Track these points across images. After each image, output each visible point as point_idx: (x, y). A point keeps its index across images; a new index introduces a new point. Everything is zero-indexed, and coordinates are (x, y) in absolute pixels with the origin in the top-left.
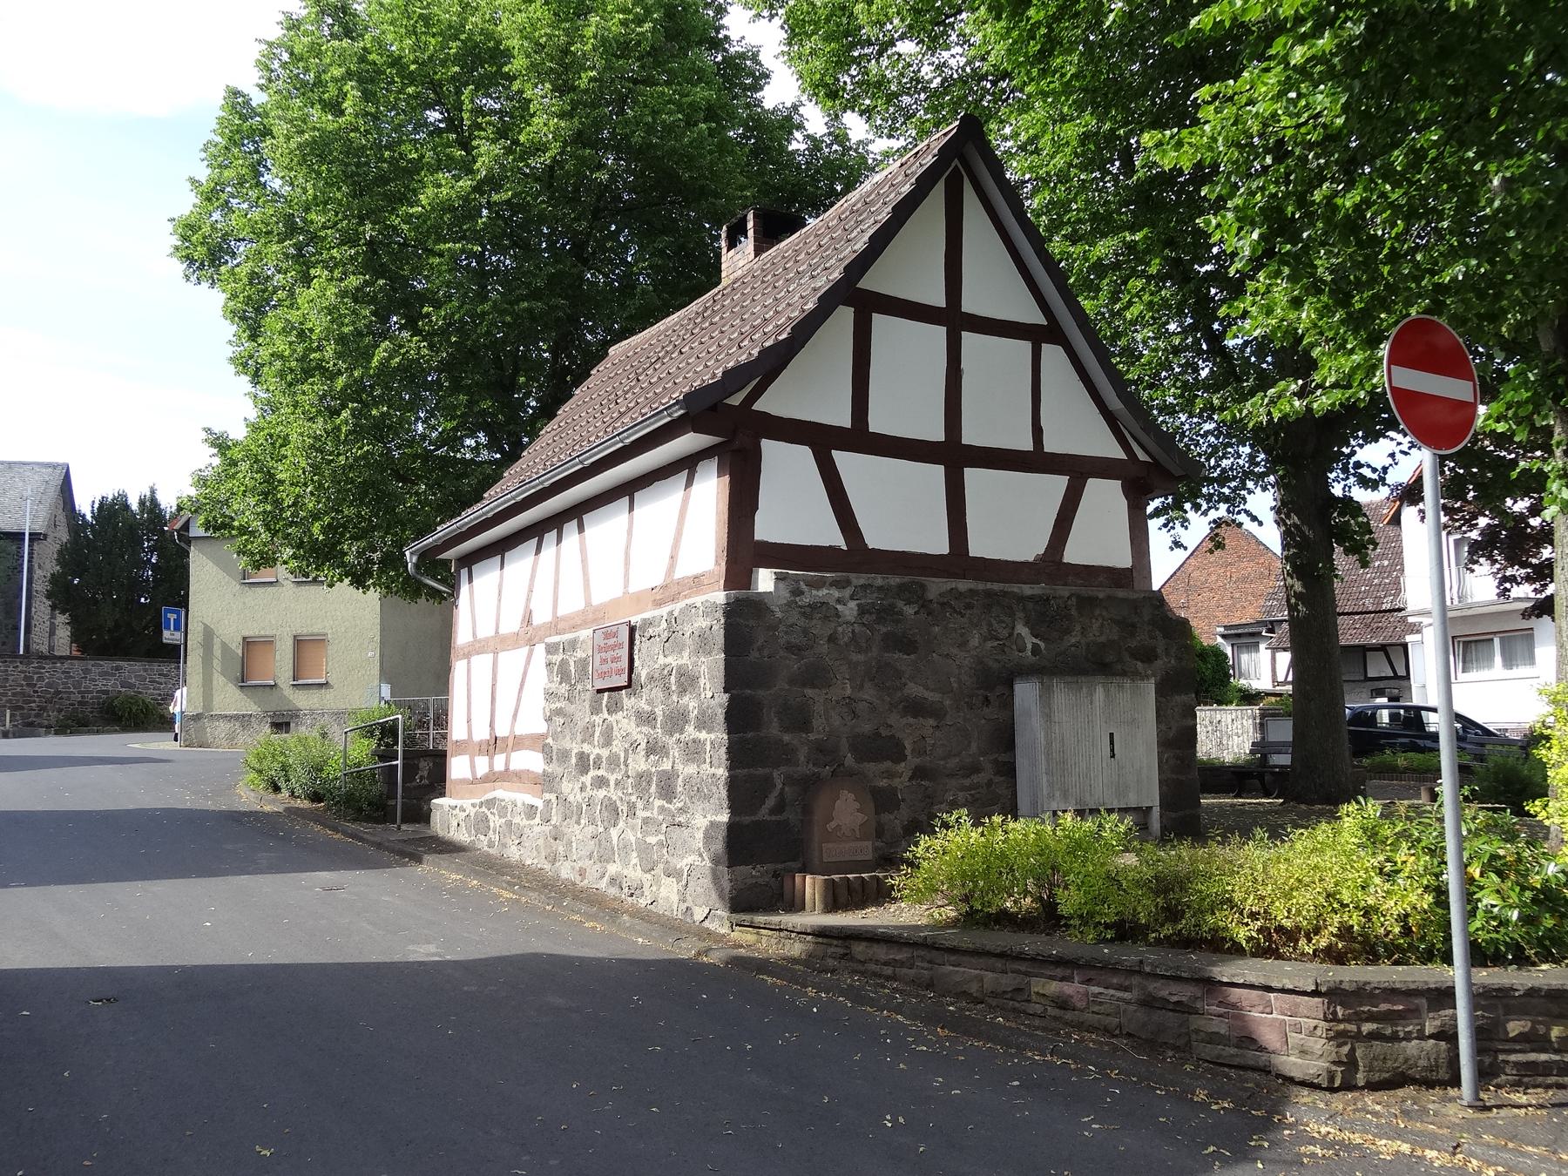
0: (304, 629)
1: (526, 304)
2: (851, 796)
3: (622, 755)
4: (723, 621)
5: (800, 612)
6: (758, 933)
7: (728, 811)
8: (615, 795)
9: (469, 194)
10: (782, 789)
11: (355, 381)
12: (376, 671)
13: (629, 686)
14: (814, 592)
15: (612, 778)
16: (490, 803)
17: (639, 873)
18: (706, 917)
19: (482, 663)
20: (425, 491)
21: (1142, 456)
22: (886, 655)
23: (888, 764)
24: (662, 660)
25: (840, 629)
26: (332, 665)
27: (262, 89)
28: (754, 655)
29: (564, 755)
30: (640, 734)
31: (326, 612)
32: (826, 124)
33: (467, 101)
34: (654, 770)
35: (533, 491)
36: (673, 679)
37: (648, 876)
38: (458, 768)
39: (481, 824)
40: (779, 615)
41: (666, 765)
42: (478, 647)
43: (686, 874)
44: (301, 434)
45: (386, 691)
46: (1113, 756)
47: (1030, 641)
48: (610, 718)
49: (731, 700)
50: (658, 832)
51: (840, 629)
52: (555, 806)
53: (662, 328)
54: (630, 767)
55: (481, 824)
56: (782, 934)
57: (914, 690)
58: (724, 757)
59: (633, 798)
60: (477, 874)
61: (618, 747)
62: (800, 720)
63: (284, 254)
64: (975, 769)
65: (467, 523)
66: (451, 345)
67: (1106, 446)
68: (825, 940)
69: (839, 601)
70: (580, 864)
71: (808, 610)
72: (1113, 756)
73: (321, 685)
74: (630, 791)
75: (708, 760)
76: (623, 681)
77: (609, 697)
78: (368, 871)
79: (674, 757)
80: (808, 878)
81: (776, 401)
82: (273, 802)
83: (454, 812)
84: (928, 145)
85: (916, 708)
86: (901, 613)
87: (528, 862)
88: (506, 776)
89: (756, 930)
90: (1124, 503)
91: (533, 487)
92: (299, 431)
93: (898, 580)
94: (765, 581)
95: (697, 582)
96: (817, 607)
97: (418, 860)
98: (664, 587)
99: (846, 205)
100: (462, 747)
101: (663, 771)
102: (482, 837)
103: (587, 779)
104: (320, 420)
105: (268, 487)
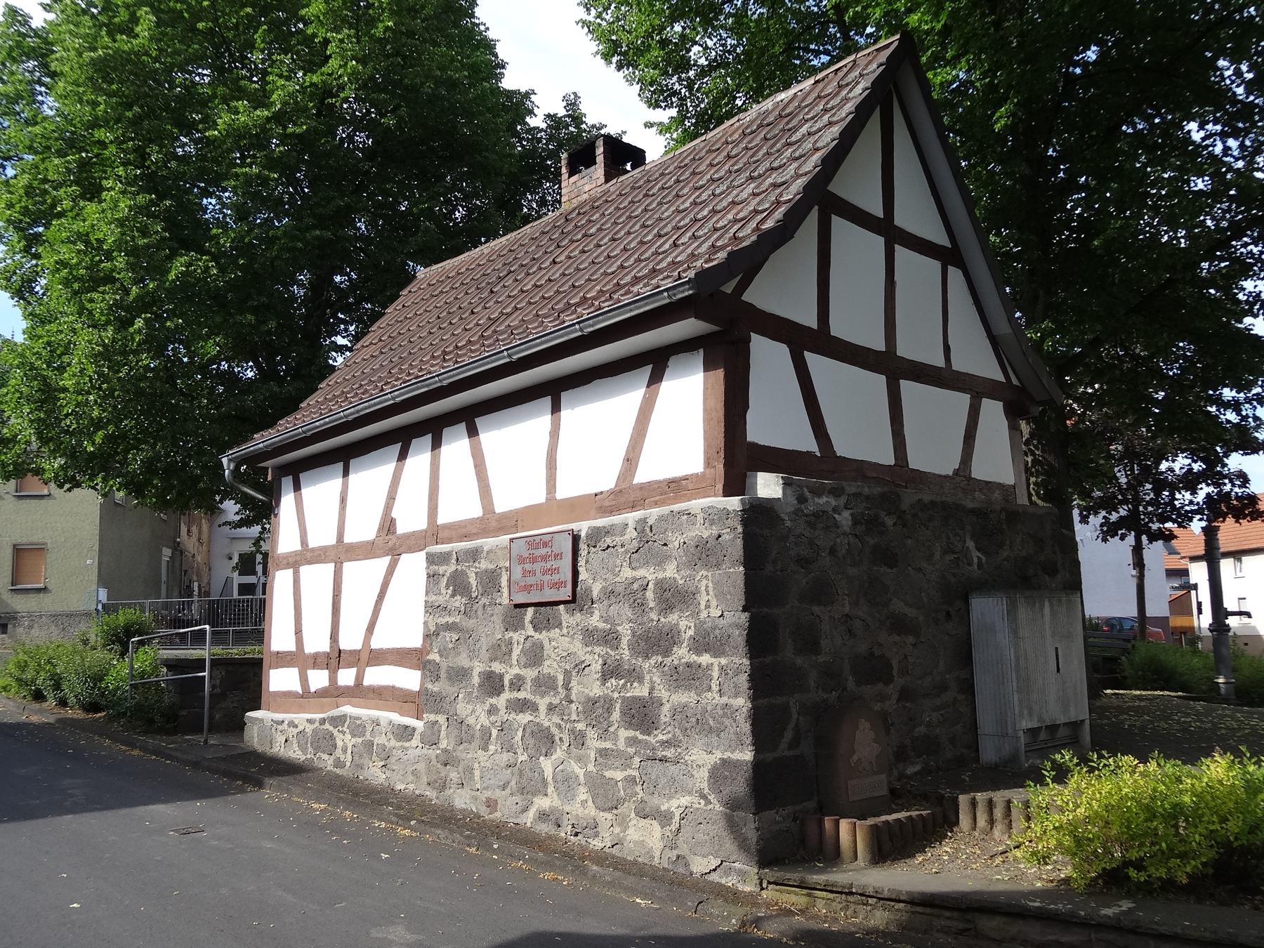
0: (23, 538)
1: (318, 232)
2: (867, 725)
3: (560, 678)
4: (740, 529)
5: (806, 522)
6: (809, 895)
7: (751, 748)
8: (544, 719)
9: (265, 124)
10: (798, 719)
11: (148, 293)
12: (94, 577)
13: (573, 600)
14: (816, 500)
16: (338, 721)
17: (591, 810)
18: (714, 870)
19: (317, 577)
20: (207, 405)
21: (1015, 381)
22: (875, 568)
23: (880, 686)
24: (627, 573)
25: (838, 540)
26: (50, 572)
27: (45, 8)
28: (769, 568)
29: (460, 675)
31: (47, 524)
32: (565, 107)
33: (259, 40)
34: (616, 695)
35: (426, 389)
36: (650, 594)
38: (280, 680)
39: (325, 742)
40: (788, 524)
42: (295, 562)
43: (677, 818)
44: (90, 342)
45: (103, 595)
46: (1058, 670)
47: (976, 554)
49: (752, 620)
50: (626, 766)
51: (838, 540)
52: (444, 728)
53: (486, 251)
54: (574, 692)
55: (325, 742)
56: (850, 898)
57: (898, 606)
58: (746, 685)
59: (580, 726)
60: (349, 805)
61: (551, 667)
62: (809, 641)
63: (66, 168)
64: (943, 688)
65: (317, 427)
66: (240, 267)
67: (991, 370)
68: (928, 910)
69: (835, 510)
70: (488, 794)
71: (813, 519)
72: (1058, 670)
73: (39, 590)
74: (574, 717)
75: (715, 688)
76: (566, 593)
77: (535, 612)
78: (211, 801)
79: (652, 682)
80: (844, 825)
81: (762, 295)
82: (41, 711)
83: (280, 727)
84: (855, 61)
85: (900, 625)
86: (883, 524)
87: (400, 786)
88: (359, 692)
89: (805, 891)
90: (1004, 423)
91: (427, 386)
92: (86, 341)
93: (879, 489)
94: (768, 486)
95: (675, 487)
96: (820, 515)
97: (259, 785)
98: (614, 493)
99: (738, 124)
100: (284, 659)
101: (633, 698)
102: (325, 757)
103: (501, 701)
104: (110, 329)
105: (47, 396)
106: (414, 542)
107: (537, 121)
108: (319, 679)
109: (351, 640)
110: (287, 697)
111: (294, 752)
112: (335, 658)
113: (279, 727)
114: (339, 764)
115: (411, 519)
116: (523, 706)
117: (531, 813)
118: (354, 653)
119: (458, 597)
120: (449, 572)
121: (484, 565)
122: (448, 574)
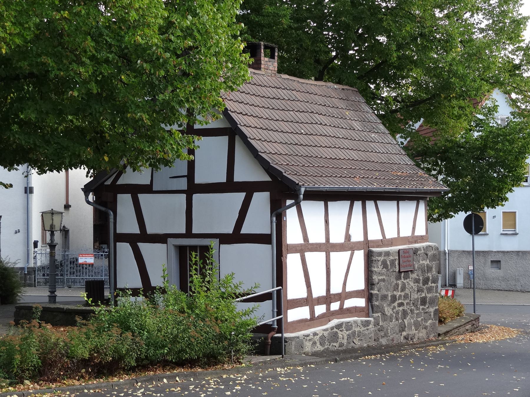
0: (501, 262)
8: (405, 308)
15: (405, 303)
30: (415, 286)
37: (417, 331)
41: (423, 295)
48: (404, 281)
83: (308, 338)
88: (342, 312)
100: (297, 303)
103: (396, 304)
107: (286, 22)
108: (320, 310)
109: (336, 289)
111: (318, 347)
112: (328, 299)
113: (308, 338)
114: (341, 345)
115: (357, 236)
118: (339, 294)
120: (382, 259)
121: (391, 258)
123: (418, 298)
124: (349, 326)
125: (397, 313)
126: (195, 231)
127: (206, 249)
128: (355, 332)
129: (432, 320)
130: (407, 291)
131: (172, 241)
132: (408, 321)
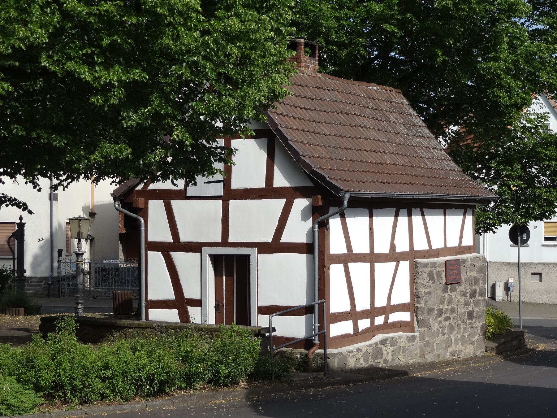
30: (462, 299)
83: (352, 354)
87: (410, 362)
88: (387, 327)
100: (340, 317)
103: (442, 318)
106: (402, 257)
108: (364, 324)
110: (345, 339)
112: (372, 313)
114: (386, 361)
116: (447, 319)
117: (448, 354)
119: (431, 281)
122: (427, 272)
123: (465, 312)
124: (394, 342)
125: (444, 327)
126: (231, 239)
127: (246, 259)
128: (400, 347)
129: (479, 335)
130: (454, 305)
131: (206, 250)
132: (454, 336)
